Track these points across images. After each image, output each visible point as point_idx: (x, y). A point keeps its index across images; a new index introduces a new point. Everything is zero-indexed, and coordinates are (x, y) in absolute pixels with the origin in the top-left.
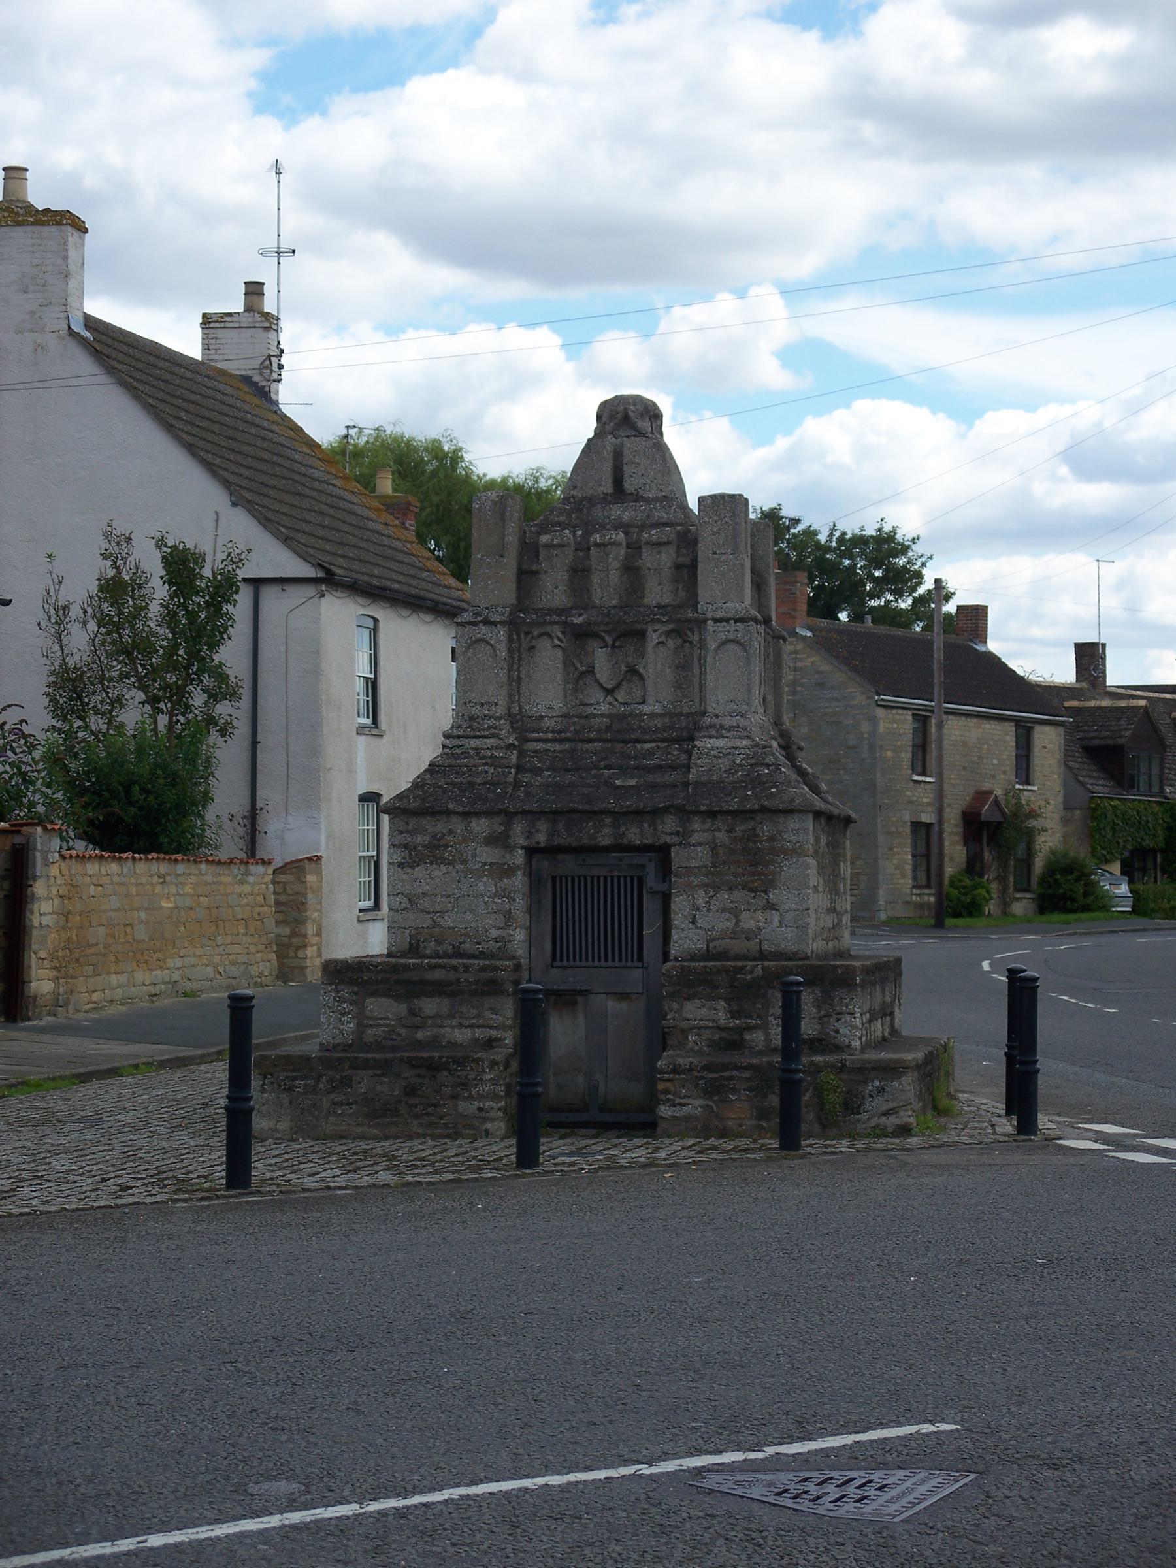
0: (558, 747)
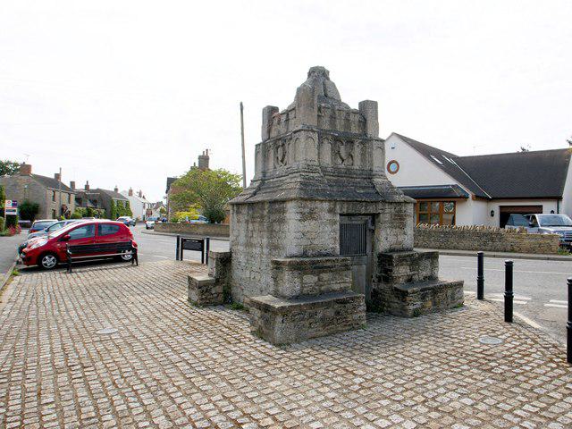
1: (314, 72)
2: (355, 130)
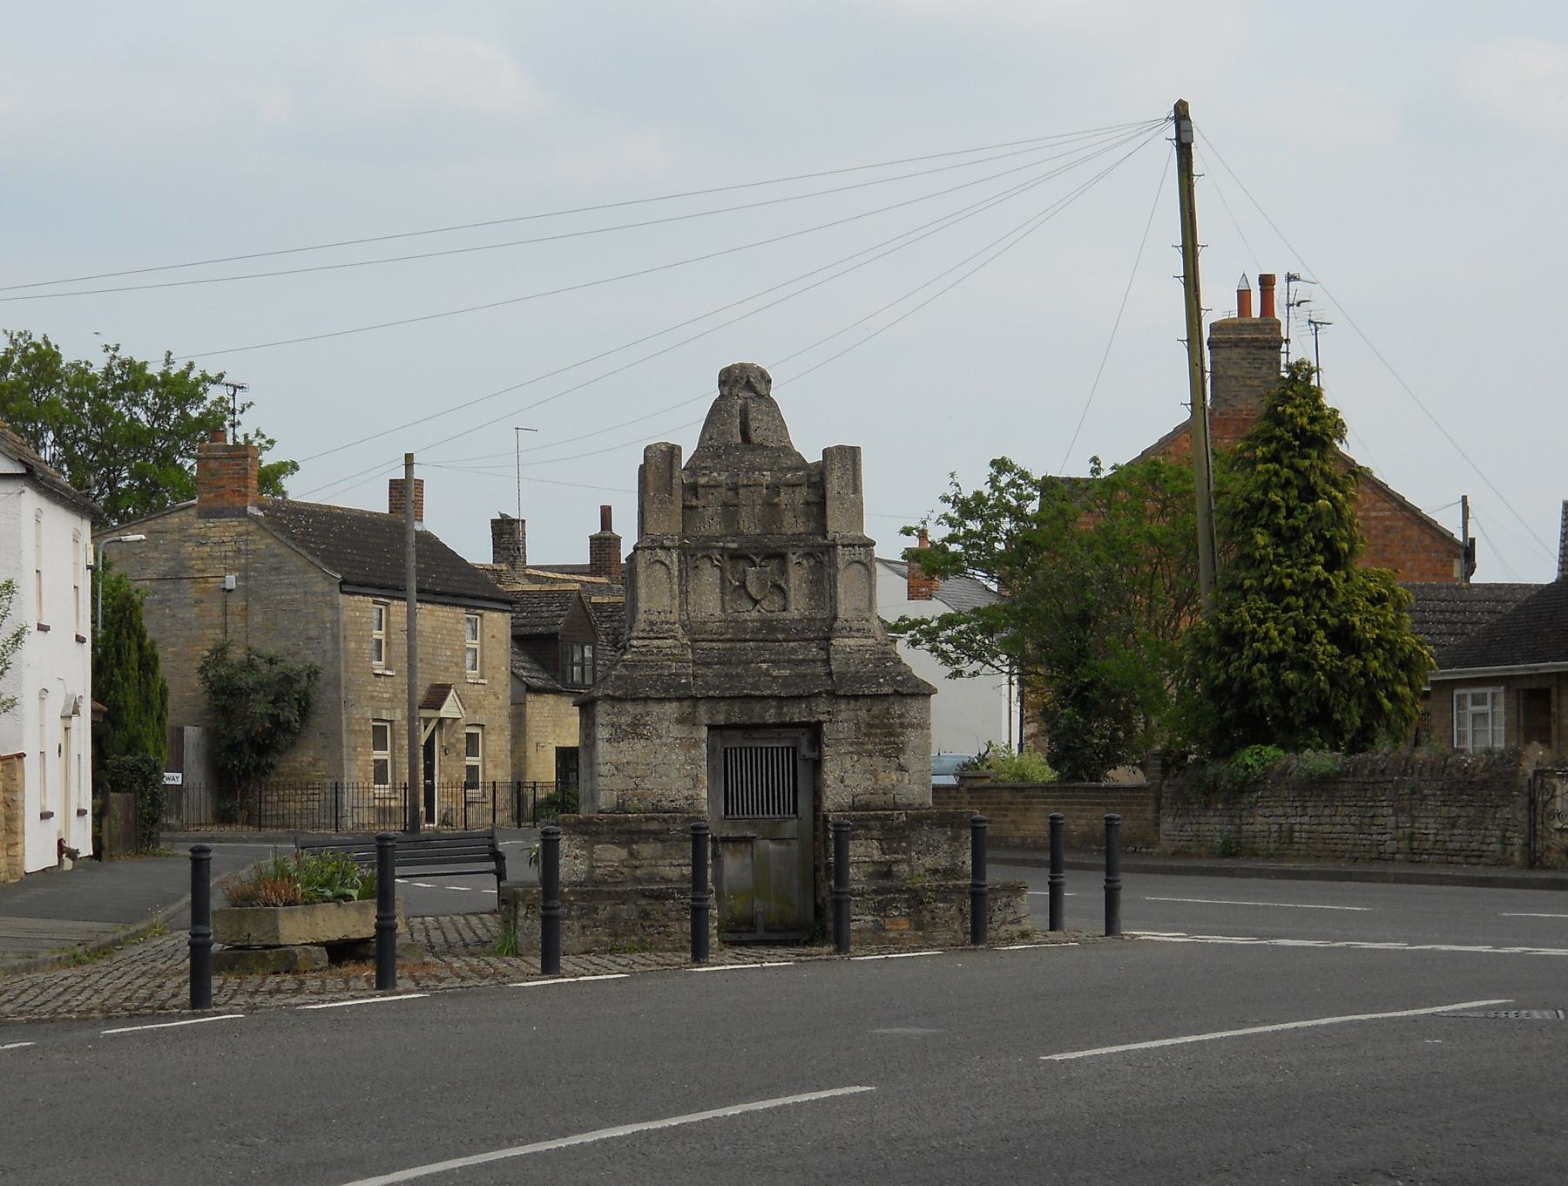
0: (720, 645)
1: (749, 386)
2: (793, 525)
